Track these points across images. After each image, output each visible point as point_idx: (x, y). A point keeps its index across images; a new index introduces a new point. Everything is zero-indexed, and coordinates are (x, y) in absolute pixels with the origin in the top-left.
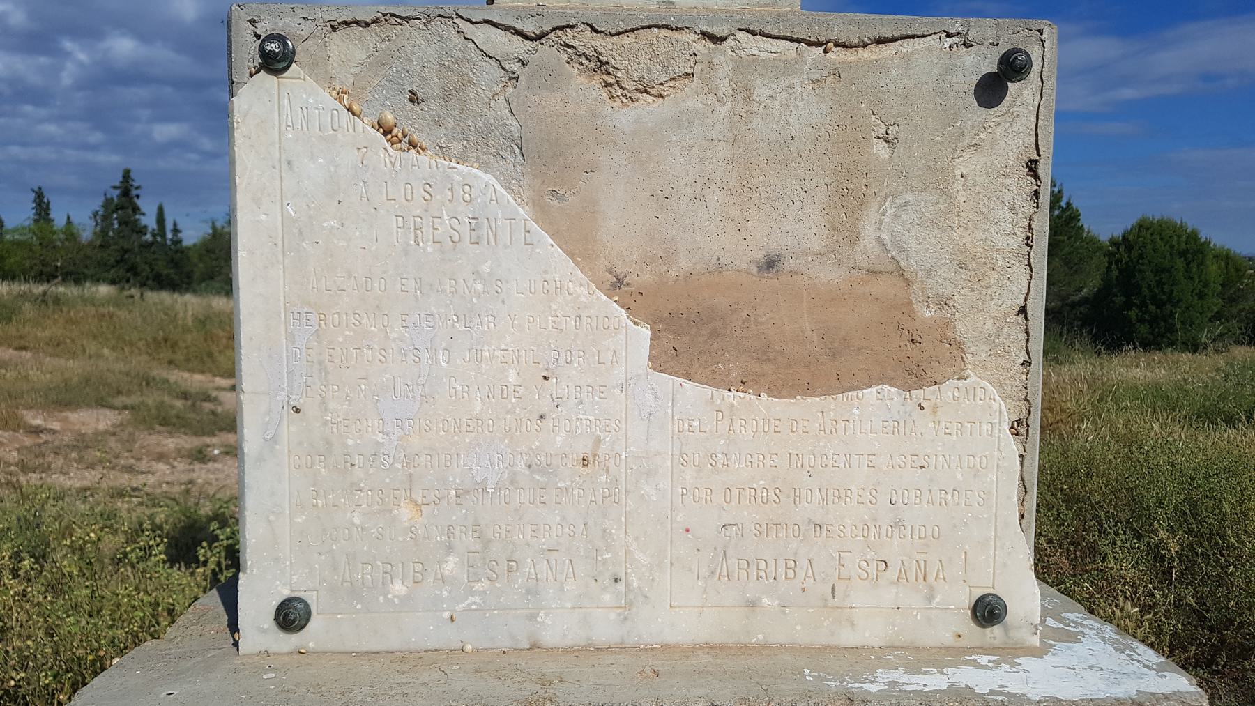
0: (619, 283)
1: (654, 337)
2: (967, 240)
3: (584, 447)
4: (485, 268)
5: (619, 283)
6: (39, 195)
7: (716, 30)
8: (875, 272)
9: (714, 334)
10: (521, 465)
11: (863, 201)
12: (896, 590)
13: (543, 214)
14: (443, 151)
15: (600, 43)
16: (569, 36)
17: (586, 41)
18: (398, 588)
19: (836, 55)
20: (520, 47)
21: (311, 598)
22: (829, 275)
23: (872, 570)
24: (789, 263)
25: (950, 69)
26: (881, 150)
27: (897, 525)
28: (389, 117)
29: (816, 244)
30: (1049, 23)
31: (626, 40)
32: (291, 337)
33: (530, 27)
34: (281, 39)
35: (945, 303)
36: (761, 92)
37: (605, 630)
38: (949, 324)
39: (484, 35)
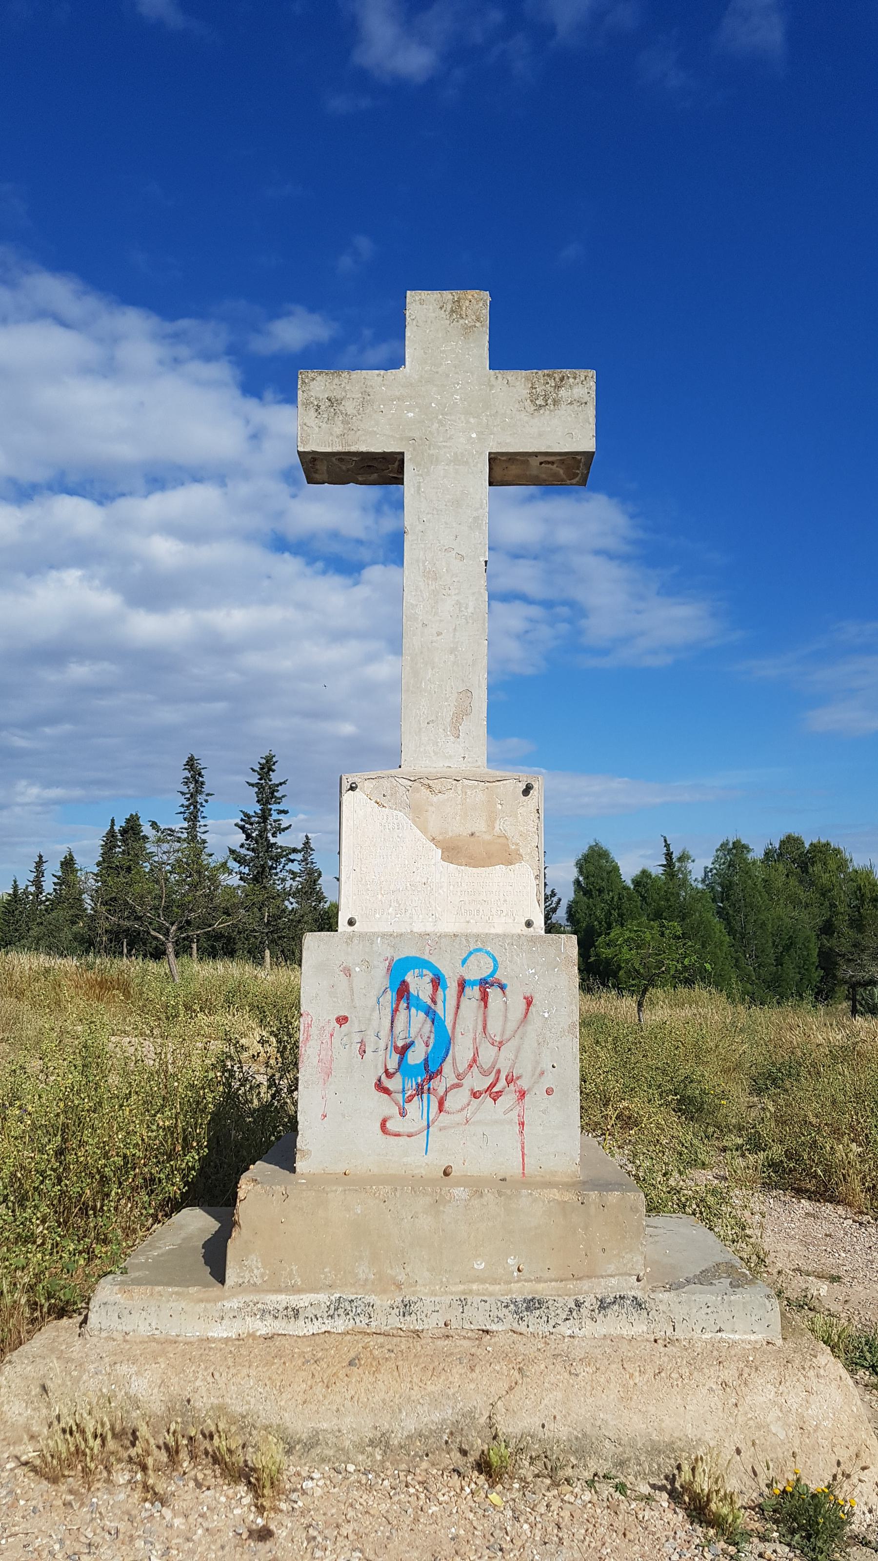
0: (434, 839)
1: (443, 852)
2: (522, 829)
3: (424, 880)
4: (400, 835)
5: (434, 839)
6: (191, 764)
7: (457, 779)
8: (506, 1010)
9: (458, 852)
10: (408, 885)
11: (496, 819)
12: (250, 1448)
13: (414, 822)
14: (391, 808)
15: (429, 782)
16: (422, 780)
17: (426, 782)
18: (377, 916)
19: (488, 784)
20: (410, 783)
21: (356, 918)
22: (487, 837)
23: (499, 913)
24: (477, 834)
25: (515, 787)
26: (499, 807)
27: (505, 901)
28: (378, 800)
29: (484, 830)
30: (544, 771)
31: (435, 781)
32: (354, 852)
33: (412, 779)
34: (354, 783)
35: (517, 844)
36: (469, 793)
37: (429, 929)
38: (518, 850)
39: (401, 781)
